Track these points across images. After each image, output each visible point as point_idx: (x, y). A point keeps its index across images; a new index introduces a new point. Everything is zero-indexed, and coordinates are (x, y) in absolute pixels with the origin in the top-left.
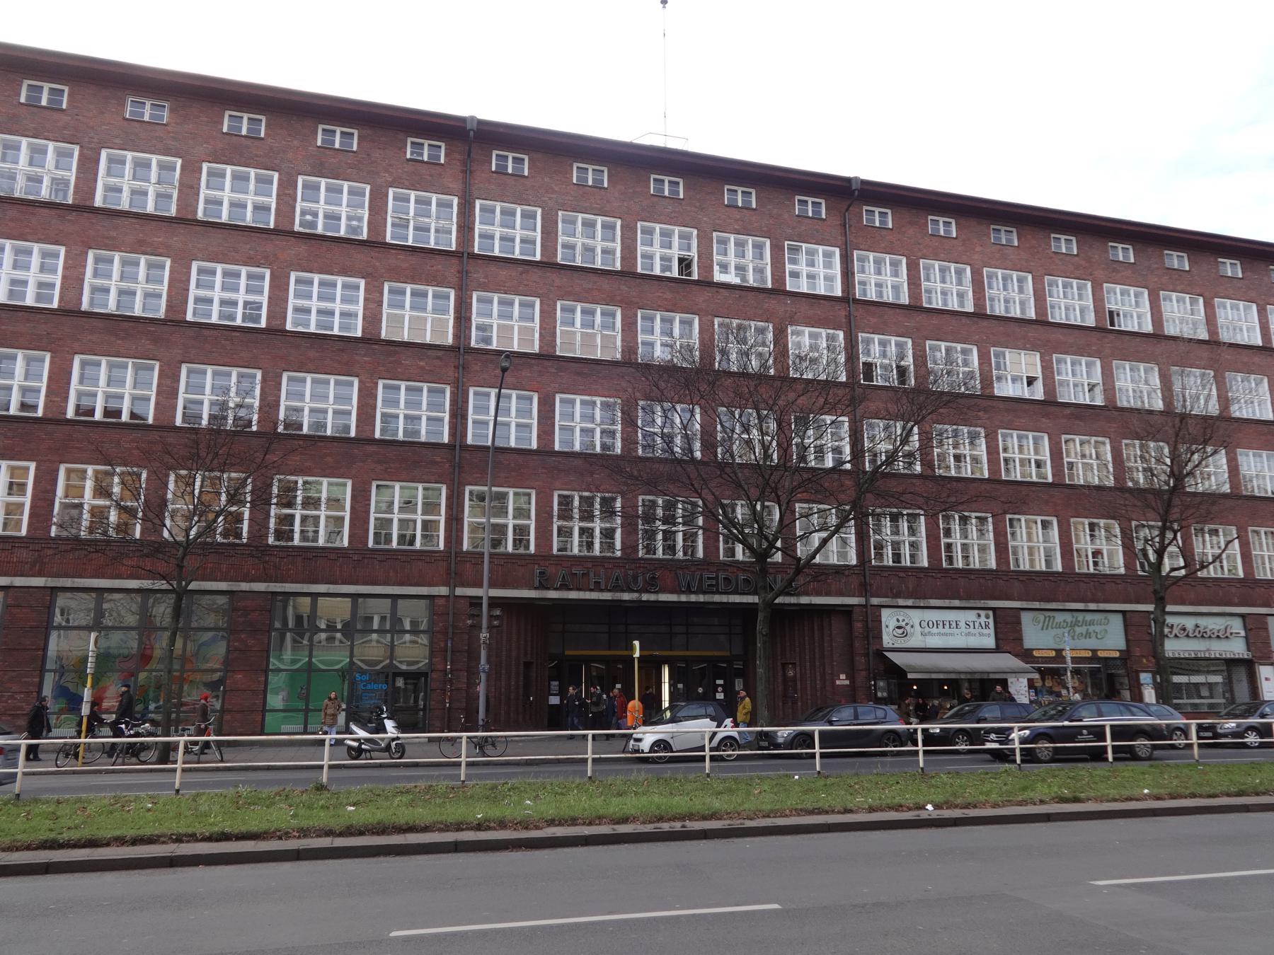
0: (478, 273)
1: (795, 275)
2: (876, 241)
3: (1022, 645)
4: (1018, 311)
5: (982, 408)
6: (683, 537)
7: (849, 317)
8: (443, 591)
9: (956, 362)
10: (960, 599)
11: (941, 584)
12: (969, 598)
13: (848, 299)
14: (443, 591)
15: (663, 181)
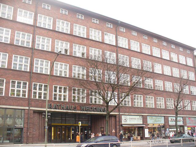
0: (38, 31)
1: (91, 36)
2: (122, 34)
3: (147, 123)
4: (125, 46)
5: (153, 75)
6: (81, 98)
7: (117, 50)
8: (27, 108)
9: (148, 66)
10: (137, 113)
11: (134, 110)
12: (138, 113)
13: (116, 46)
14: (27, 108)
15: (79, 15)
